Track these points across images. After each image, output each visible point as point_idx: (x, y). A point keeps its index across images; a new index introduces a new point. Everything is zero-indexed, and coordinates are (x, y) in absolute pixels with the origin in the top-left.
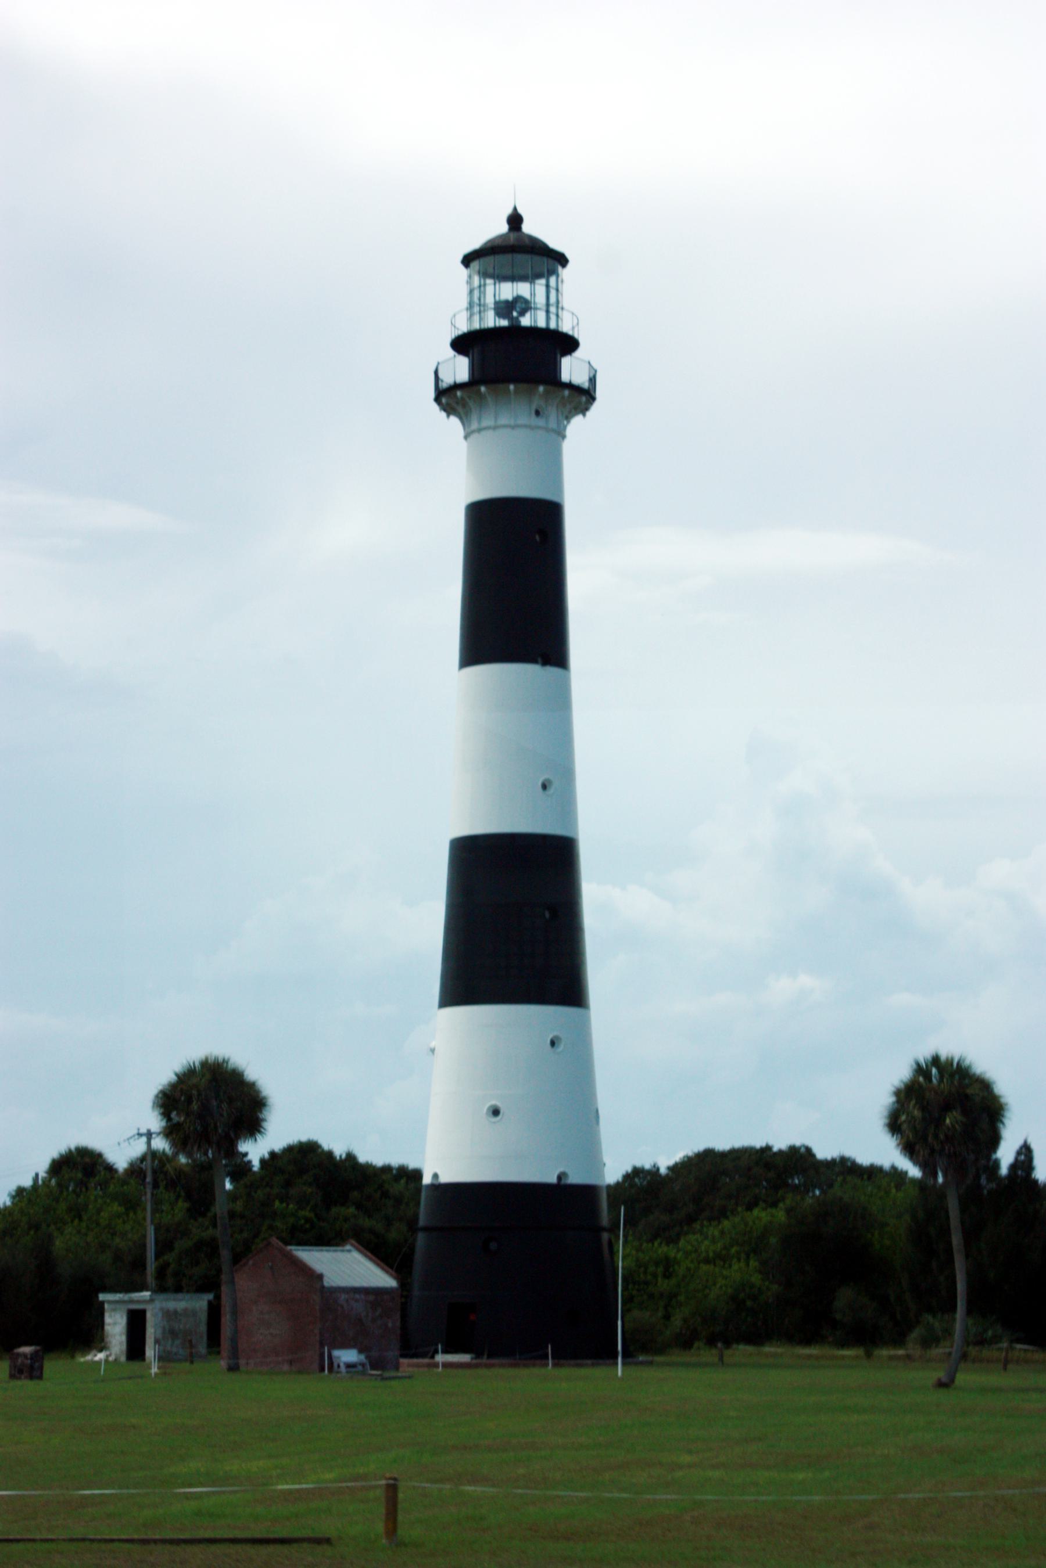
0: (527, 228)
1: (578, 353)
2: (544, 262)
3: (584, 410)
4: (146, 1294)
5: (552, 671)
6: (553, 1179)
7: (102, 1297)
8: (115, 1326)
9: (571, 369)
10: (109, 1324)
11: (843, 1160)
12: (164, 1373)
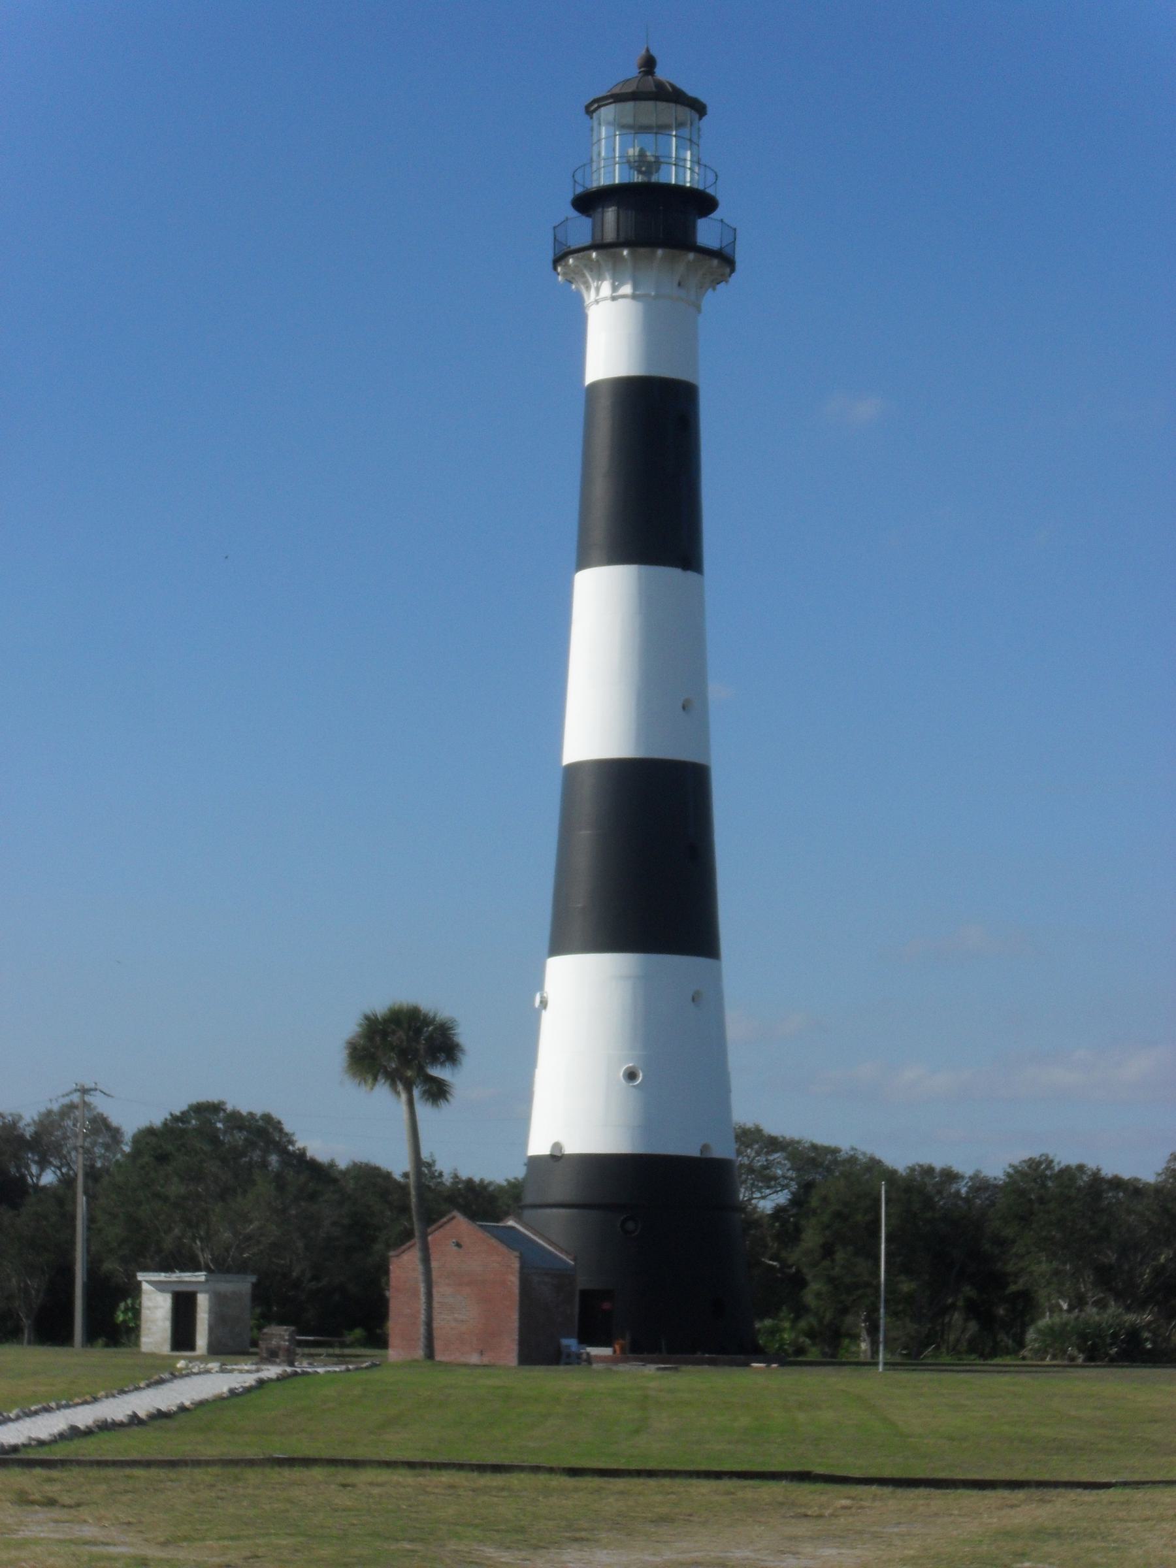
0: (662, 73)
1: (715, 215)
2: (685, 113)
3: (722, 279)
4: (201, 1276)
5: (691, 575)
6: (695, 1152)
7: (141, 1276)
8: (156, 1308)
9: (707, 232)
10: (149, 1308)
11: (279, 1122)
12: (884, 1370)
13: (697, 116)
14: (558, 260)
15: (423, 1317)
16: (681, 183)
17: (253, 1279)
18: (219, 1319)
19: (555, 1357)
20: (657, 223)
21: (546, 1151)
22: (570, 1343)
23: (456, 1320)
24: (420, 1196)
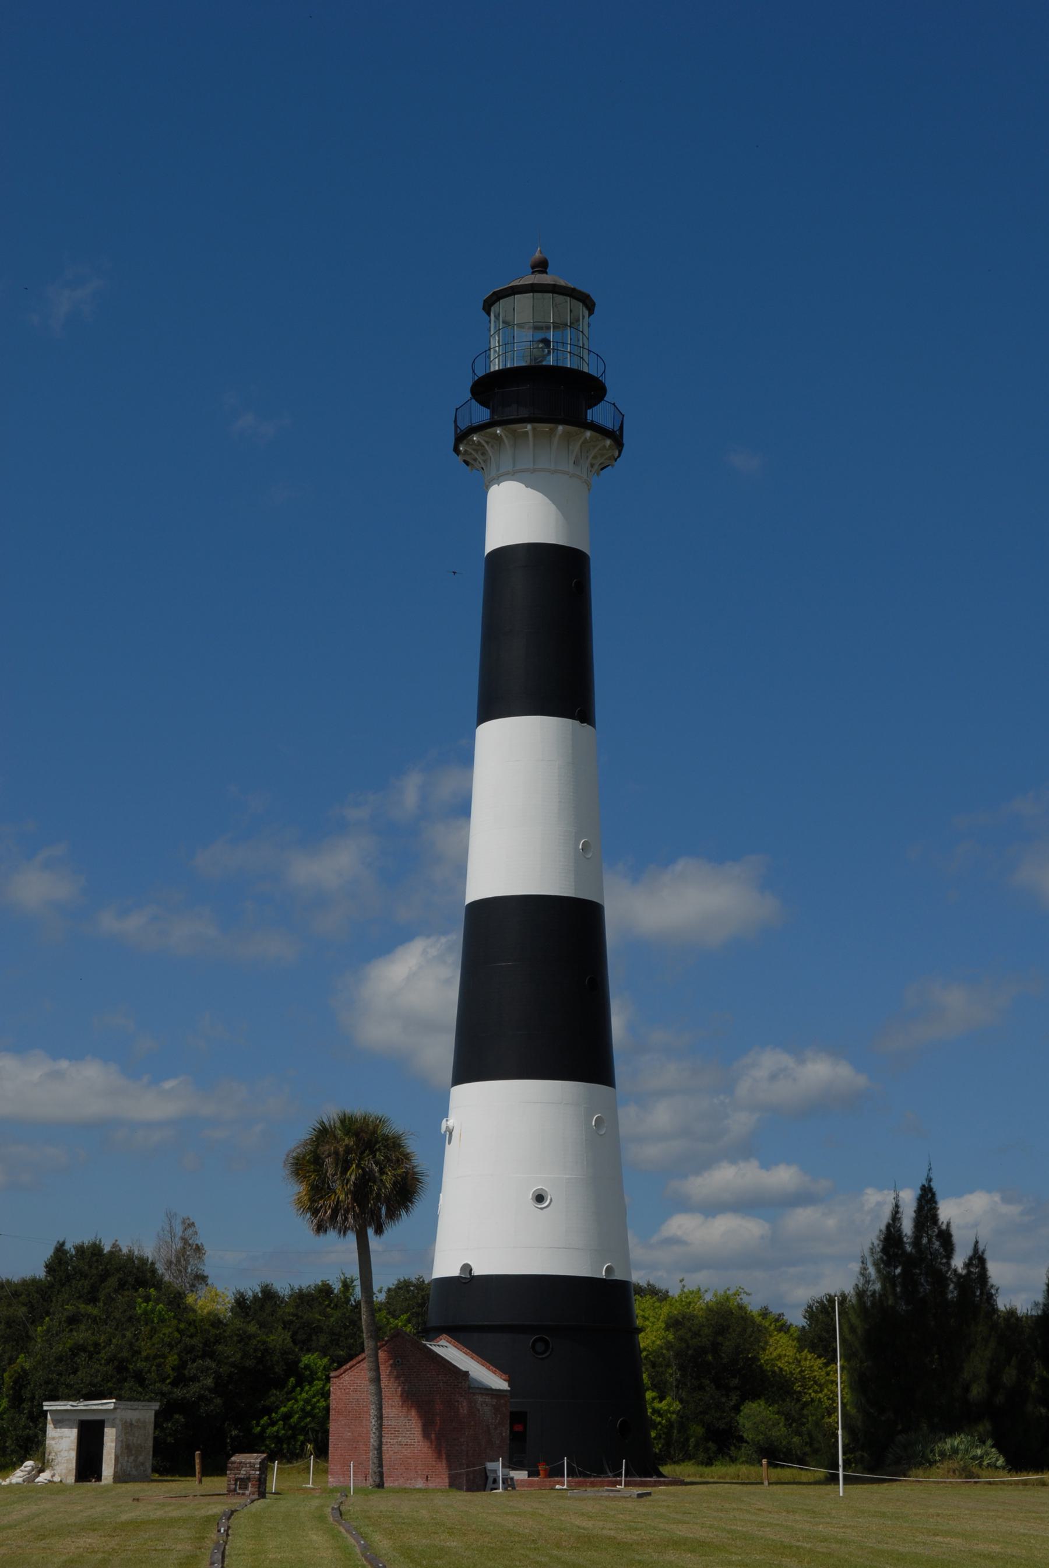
4: (109, 1404)
7: (47, 1406)
10: (53, 1439)
13: (586, 313)
14: (461, 437)
15: (373, 1441)
16: (560, 364)
17: (156, 1406)
18: (125, 1449)
19: (481, 1482)
20: (543, 402)
21: (455, 1272)
22: (498, 1467)
23: (400, 1444)
24: (841, 1303)
